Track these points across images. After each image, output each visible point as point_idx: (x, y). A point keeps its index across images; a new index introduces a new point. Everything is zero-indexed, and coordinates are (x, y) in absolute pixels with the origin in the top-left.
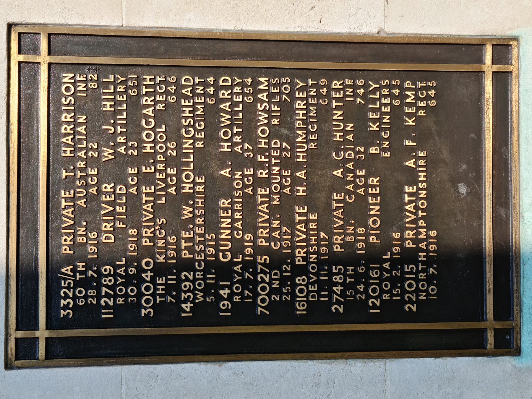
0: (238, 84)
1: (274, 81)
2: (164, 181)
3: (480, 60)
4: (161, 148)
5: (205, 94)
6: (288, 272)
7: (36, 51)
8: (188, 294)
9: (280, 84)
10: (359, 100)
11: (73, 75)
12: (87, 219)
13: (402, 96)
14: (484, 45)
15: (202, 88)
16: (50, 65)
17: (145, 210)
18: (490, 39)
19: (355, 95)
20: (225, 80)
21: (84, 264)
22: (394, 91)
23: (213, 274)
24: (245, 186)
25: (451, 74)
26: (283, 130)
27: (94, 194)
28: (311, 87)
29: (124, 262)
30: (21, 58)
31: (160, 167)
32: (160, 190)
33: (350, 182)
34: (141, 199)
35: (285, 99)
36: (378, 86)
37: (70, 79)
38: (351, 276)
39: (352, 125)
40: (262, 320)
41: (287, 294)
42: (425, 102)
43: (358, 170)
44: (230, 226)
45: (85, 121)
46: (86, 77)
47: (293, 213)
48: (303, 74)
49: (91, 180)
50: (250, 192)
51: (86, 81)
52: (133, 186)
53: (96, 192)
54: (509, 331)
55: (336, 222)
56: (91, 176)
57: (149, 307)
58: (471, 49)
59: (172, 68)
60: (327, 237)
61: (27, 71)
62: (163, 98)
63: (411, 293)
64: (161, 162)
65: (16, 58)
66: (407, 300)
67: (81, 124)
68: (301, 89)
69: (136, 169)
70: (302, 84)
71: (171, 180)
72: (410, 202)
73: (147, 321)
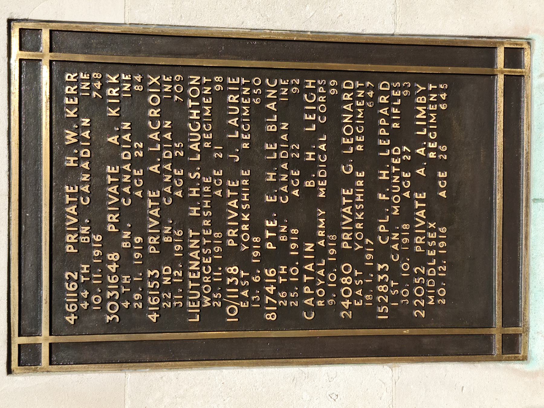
3: (492, 63)
5: (366, 98)
7: (36, 48)
9: (401, 88)
10: (176, 97)
12: (92, 219)
14: (496, 48)
15: (363, 92)
19: (91, 88)
20: (349, 84)
21: (88, 266)
24: (403, 190)
25: (467, 73)
28: (358, 89)
29: (324, 264)
31: (127, 167)
33: (167, 184)
38: (125, 286)
40: (346, 324)
42: (436, 105)
50: (220, 195)
53: (117, 191)
57: (115, 314)
61: (29, 68)
63: (419, 298)
68: (422, 93)
70: (422, 88)
72: (347, 205)
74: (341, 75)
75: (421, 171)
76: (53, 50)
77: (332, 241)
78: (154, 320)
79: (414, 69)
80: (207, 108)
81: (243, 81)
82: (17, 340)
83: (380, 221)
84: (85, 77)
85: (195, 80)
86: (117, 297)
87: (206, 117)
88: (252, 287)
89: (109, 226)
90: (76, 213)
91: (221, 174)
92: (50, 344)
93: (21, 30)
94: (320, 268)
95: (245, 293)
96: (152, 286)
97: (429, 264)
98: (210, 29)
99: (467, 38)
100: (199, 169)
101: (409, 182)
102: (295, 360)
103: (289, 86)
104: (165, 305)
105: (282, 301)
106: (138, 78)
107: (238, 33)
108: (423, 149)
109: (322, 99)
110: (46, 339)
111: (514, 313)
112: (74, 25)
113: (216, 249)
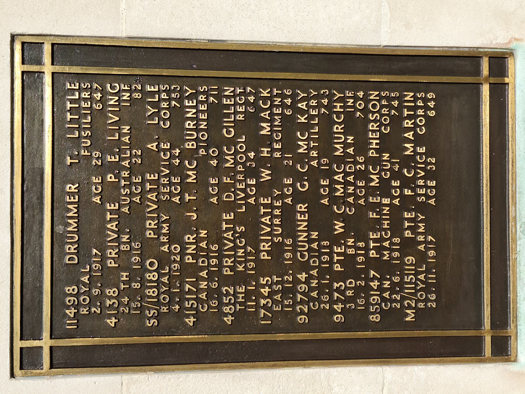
0: (277, 95)
1: (202, 89)
2: (243, 191)
3: (477, 72)
4: (241, 158)
8: (113, 301)
13: (330, 107)
17: (109, 229)
18: (486, 54)
22: (286, 101)
23: (327, 279)
25: (459, 78)
27: (97, 203)
30: (27, 68)
32: (240, 199)
34: (259, 210)
35: (175, 105)
36: (195, 91)
41: (325, 303)
44: (76, 230)
45: (129, 132)
46: (130, 87)
47: (221, 220)
50: (253, 202)
51: (130, 91)
52: (96, 195)
55: (110, 236)
58: (464, 62)
61: (31, 81)
64: (240, 172)
65: (18, 69)
66: (407, 306)
67: (125, 134)
69: (100, 178)
70: (339, 95)
71: (360, 192)
74: (258, 83)
75: (350, 179)
76: (25, 63)
78: (230, 323)
79: (115, 71)
82: (18, 344)
84: (126, 88)
85: (374, 95)
86: (233, 301)
88: (285, 292)
89: (148, 232)
93: (23, 43)
97: (163, 272)
100: (306, 178)
101: (398, 190)
102: (139, 368)
104: (123, 310)
105: (324, 305)
106: (361, 94)
110: (488, 332)
112: (154, 41)
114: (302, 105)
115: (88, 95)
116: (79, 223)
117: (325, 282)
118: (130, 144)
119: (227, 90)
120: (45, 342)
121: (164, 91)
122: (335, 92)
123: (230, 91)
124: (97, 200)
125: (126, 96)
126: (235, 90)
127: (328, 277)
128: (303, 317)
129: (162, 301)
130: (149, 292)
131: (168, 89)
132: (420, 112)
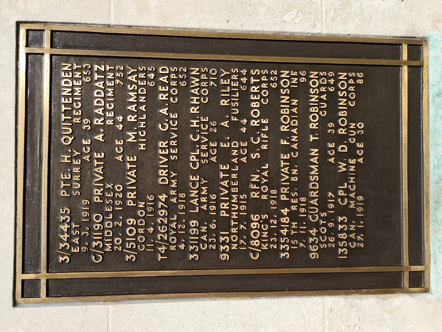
1: (173, 69)
3: (398, 55)
6: (275, 225)
7: (39, 42)
11: (199, 69)
16: (51, 56)
23: (362, 225)
25: (379, 67)
26: (271, 110)
30: (29, 50)
36: (229, 73)
37: (286, 75)
39: (296, 101)
43: (358, 144)
48: (228, 64)
49: (85, 150)
54: (35, 294)
55: (283, 177)
56: (212, 148)
58: (390, 47)
59: (167, 61)
60: (334, 196)
61: (33, 60)
62: (112, 83)
73: (285, 263)
77: (182, 199)
79: (171, 55)
80: (110, 90)
81: (108, 68)
82: (21, 277)
83: (340, 187)
85: (343, 76)
87: (109, 97)
90: (135, 176)
91: (362, 147)
92: (47, 280)
93: (27, 31)
94: (172, 221)
95: (204, 238)
96: (284, 241)
97: (233, 170)
98: (167, 29)
99: (152, 28)
103: (299, 76)
104: (117, 249)
106: (244, 72)
107: (228, 34)
108: (226, 122)
109: (352, 89)
111: (418, 253)
113: (212, 208)
114: (132, 78)
115: (144, 76)
116: (105, 176)
117: (360, 226)
118: (137, 112)
119: (312, 74)
120: (43, 276)
121: (174, 72)
122: (222, 70)
123: (343, 76)
124: (332, 160)
125: (295, 80)
126: (200, 70)
127: (362, 222)
128: (225, 255)
129: (171, 240)
130: (341, 236)
131: (177, 70)
132: (264, 86)
